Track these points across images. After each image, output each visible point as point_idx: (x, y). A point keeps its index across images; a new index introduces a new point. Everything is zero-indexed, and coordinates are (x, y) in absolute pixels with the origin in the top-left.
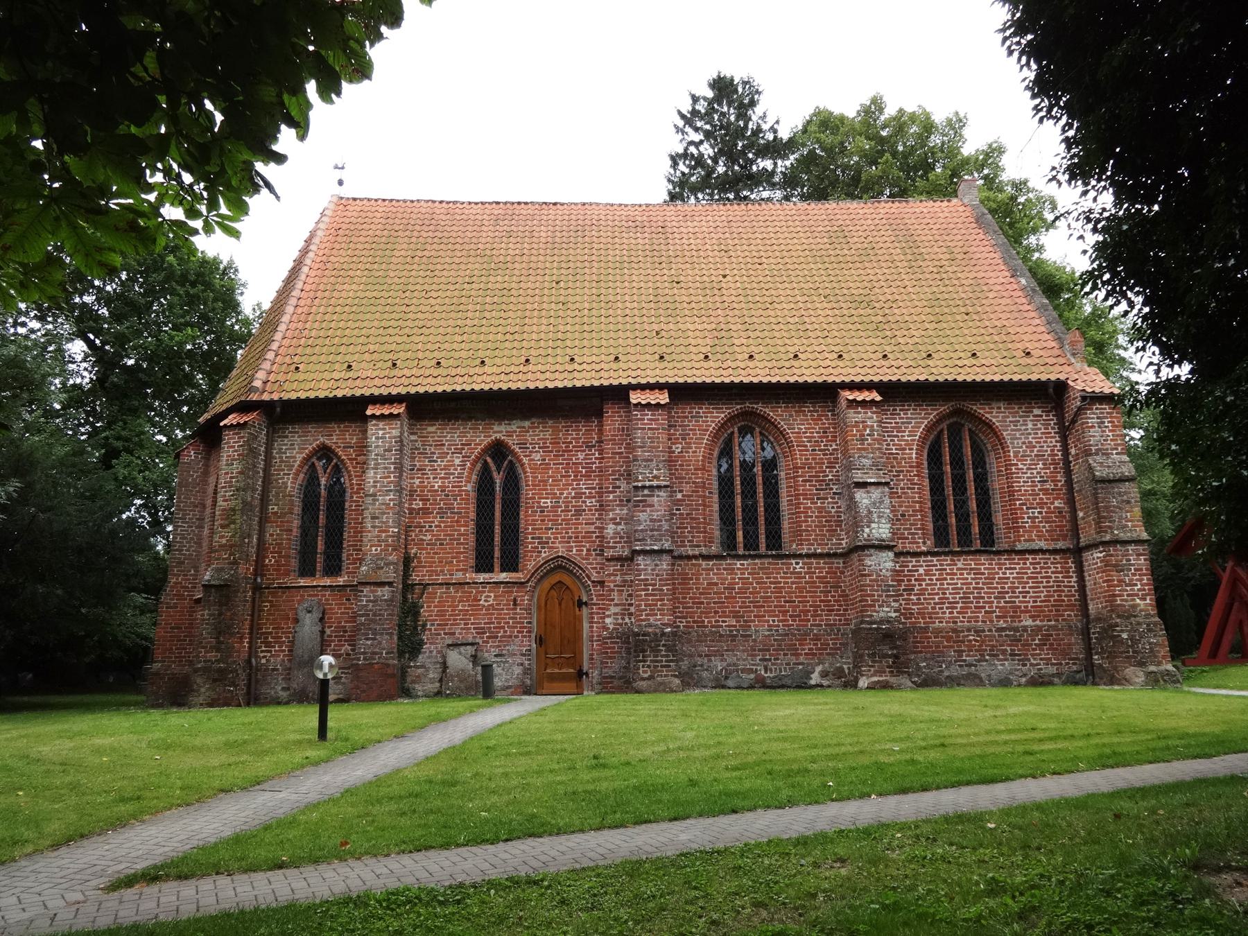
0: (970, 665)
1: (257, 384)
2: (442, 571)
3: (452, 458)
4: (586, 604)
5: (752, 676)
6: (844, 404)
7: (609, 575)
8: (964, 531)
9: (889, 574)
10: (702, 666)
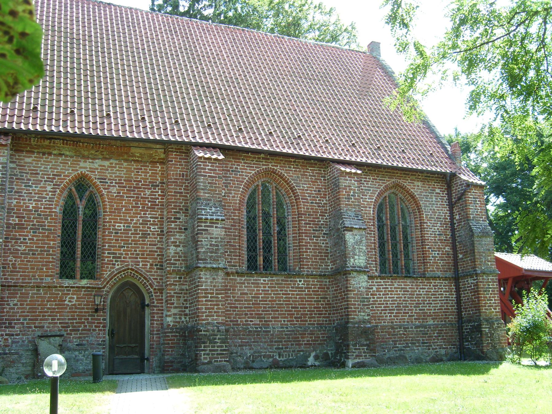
4: (148, 305)
5: (271, 360)
7: (171, 285)
10: (236, 353)
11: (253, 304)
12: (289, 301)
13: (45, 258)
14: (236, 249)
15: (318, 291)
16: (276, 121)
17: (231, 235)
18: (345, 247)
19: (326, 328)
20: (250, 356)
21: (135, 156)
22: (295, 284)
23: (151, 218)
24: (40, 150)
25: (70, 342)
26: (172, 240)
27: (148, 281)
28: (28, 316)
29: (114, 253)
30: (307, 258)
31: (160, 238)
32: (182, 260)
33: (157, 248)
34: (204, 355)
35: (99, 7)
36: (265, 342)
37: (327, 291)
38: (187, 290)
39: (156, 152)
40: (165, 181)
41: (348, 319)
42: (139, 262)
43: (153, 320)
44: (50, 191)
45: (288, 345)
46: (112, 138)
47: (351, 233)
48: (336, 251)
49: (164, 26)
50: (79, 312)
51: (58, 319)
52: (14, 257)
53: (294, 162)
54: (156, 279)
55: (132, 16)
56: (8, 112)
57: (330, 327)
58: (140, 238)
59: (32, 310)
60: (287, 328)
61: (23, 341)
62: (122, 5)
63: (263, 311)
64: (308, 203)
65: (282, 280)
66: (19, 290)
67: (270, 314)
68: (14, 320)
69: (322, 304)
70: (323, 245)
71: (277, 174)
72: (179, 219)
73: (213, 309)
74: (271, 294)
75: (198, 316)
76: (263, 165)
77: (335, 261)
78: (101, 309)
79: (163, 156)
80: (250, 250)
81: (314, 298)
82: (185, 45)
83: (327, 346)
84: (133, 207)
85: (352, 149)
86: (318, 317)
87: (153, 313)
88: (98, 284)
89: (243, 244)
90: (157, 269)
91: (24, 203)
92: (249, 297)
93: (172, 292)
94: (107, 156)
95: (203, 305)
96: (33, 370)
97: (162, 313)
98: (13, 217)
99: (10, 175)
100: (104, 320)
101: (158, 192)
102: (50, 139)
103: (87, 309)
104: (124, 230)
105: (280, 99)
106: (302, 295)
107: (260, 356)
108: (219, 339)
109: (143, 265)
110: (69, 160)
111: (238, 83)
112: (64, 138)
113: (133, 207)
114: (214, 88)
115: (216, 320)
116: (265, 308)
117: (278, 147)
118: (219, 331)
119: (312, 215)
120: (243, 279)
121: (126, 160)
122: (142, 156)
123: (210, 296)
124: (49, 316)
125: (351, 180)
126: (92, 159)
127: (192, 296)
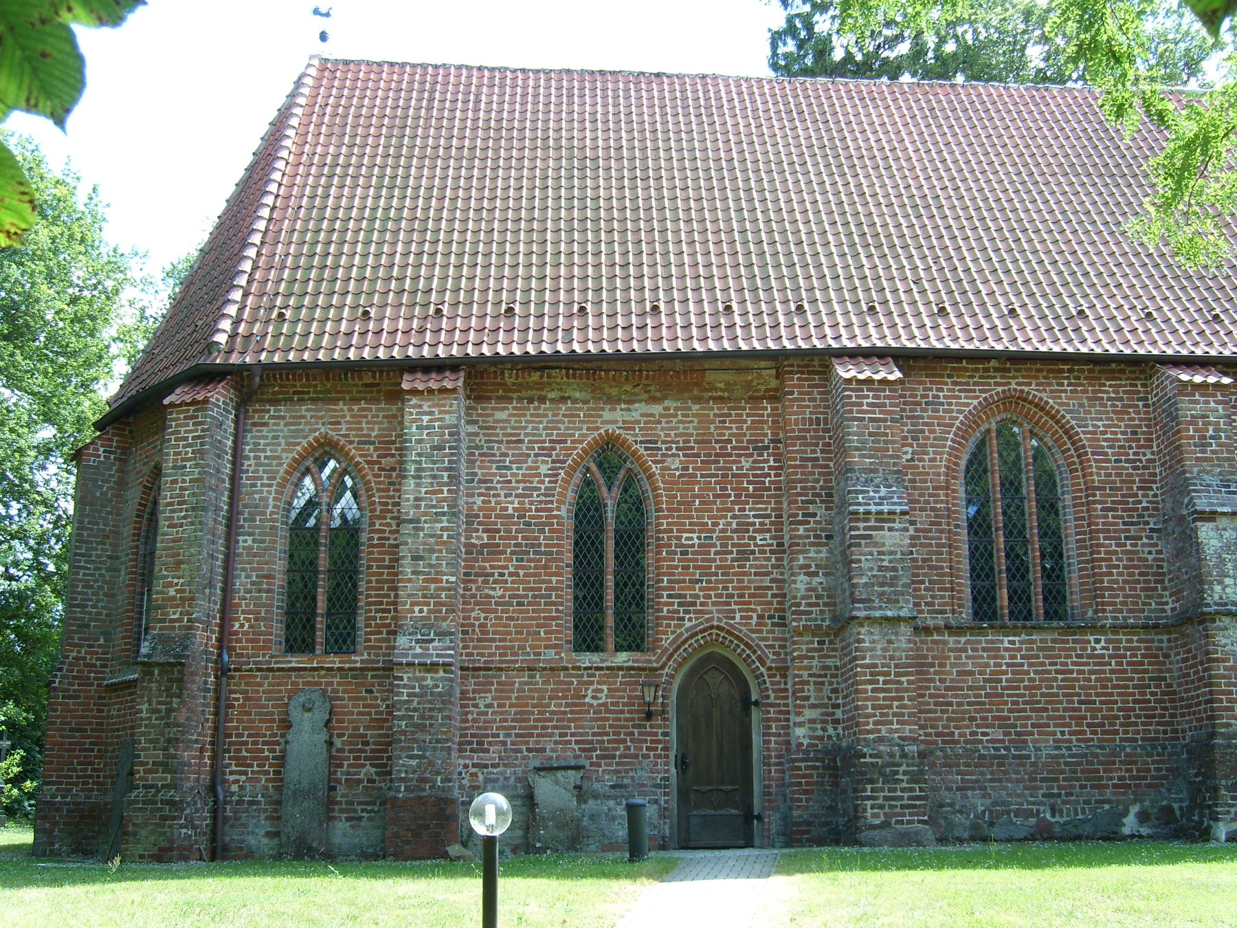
1: (221, 338)
2: (522, 648)
3: (533, 466)
4: (756, 703)
5: (1033, 821)
7: (801, 657)
8: (1019, 598)
10: (952, 805)
11: (987, 695)
12: (1073, 687)
13: (544, 611)
14: (943, 575)
15: (1142, 663)
16: (1025, 283)
17: (930, 545)
18: (1200, 560)
19: (1164, 748)
20: (983, 812)
21: (716, 389)
22: (1085, 649)
23: (754, 516)
24: (524, 394)
25: (598, 780)
26: (801, 562)
27: (754, 652)
28: (515, 728)
29: (680, 596)
30: (1112, 589)
31: (777, 559)
32: (825, 604)
33: (772, 581)
34: (872, 807)
35: (637, 84)
36: (1018, 781)
37: (1164, 663)
38: (837, 668)
39: (760, 376)
40: (781, 436)
41: (1214, 726)
42: (734, 611)
43: (769, 735)
44: (546, 476)
45: (1073, 787)
46: (663, 356)
47: (1211, 525)
48: (1179, 569)
49: (776, 104)
50: (614, 719)
51: (573, 735)
52: (483, 611)
53: (1069, 371)
54: (772, 647)
55: (706, 92)
56: (458, 325)
57: (1174, 746)
58: (733, 560)
59: (522, 717)
60: (1069, 749)
61: (506, 779)
62: (684, 72)
63: (1010, 711)
64: (1108, 461)
65: (1054, 641)
66: (494, 677)
67: (1029, 718)
68: (487, 736)
69: (1152, 694)
70: (1150, 557)
71: (1031, 403)
72: (814, 515)
73: (890, 707)
74: (1028, 673)
75: (858, 725)
76: (996, 384)
77: (1180, 591)
78: (657, 713)
79: (774, 383)
80: (978, 576)
81: (1132, 679)
82: (820, 138)
83: (1169, 790)
84: (715, 496)
85: (1211, 328)
86: (1143, 724)
87: (768, 720)
88: (649, 661)
89: (959, 562)
90: (774, 624)
91: (497, 503)
92: (977, 680)
93: (805, 674)
94: (658, 394)
95: (867, 699)
96: (525, 837)
97: (788, 720)
98: (477, 530)
99: (469, 448)
100: (666, 734)
101: (768, 461)
102: (541, 369)
103: (630, 712)
104: (700, 546)
105: (1037, 231)
106: (1104, 672)
107: (1008, 813)
108: (905, 773)
109: (742, 618)
110: (580, 409)
111: (940, 207)
112: (570, 365)
113: (715, 496)
114: (885, 225)
115: (897, 731)
116: (1016, 703)
117: (1028, 340)
118: (904, 755)
119: (1121, 489)
120: (963, 639)
121: (697, 400)
122: (729, 387)
123: (881, 679)
124: (555, 727)
125: (1207, 402)
126: (625, 402)
127: (845, 681)
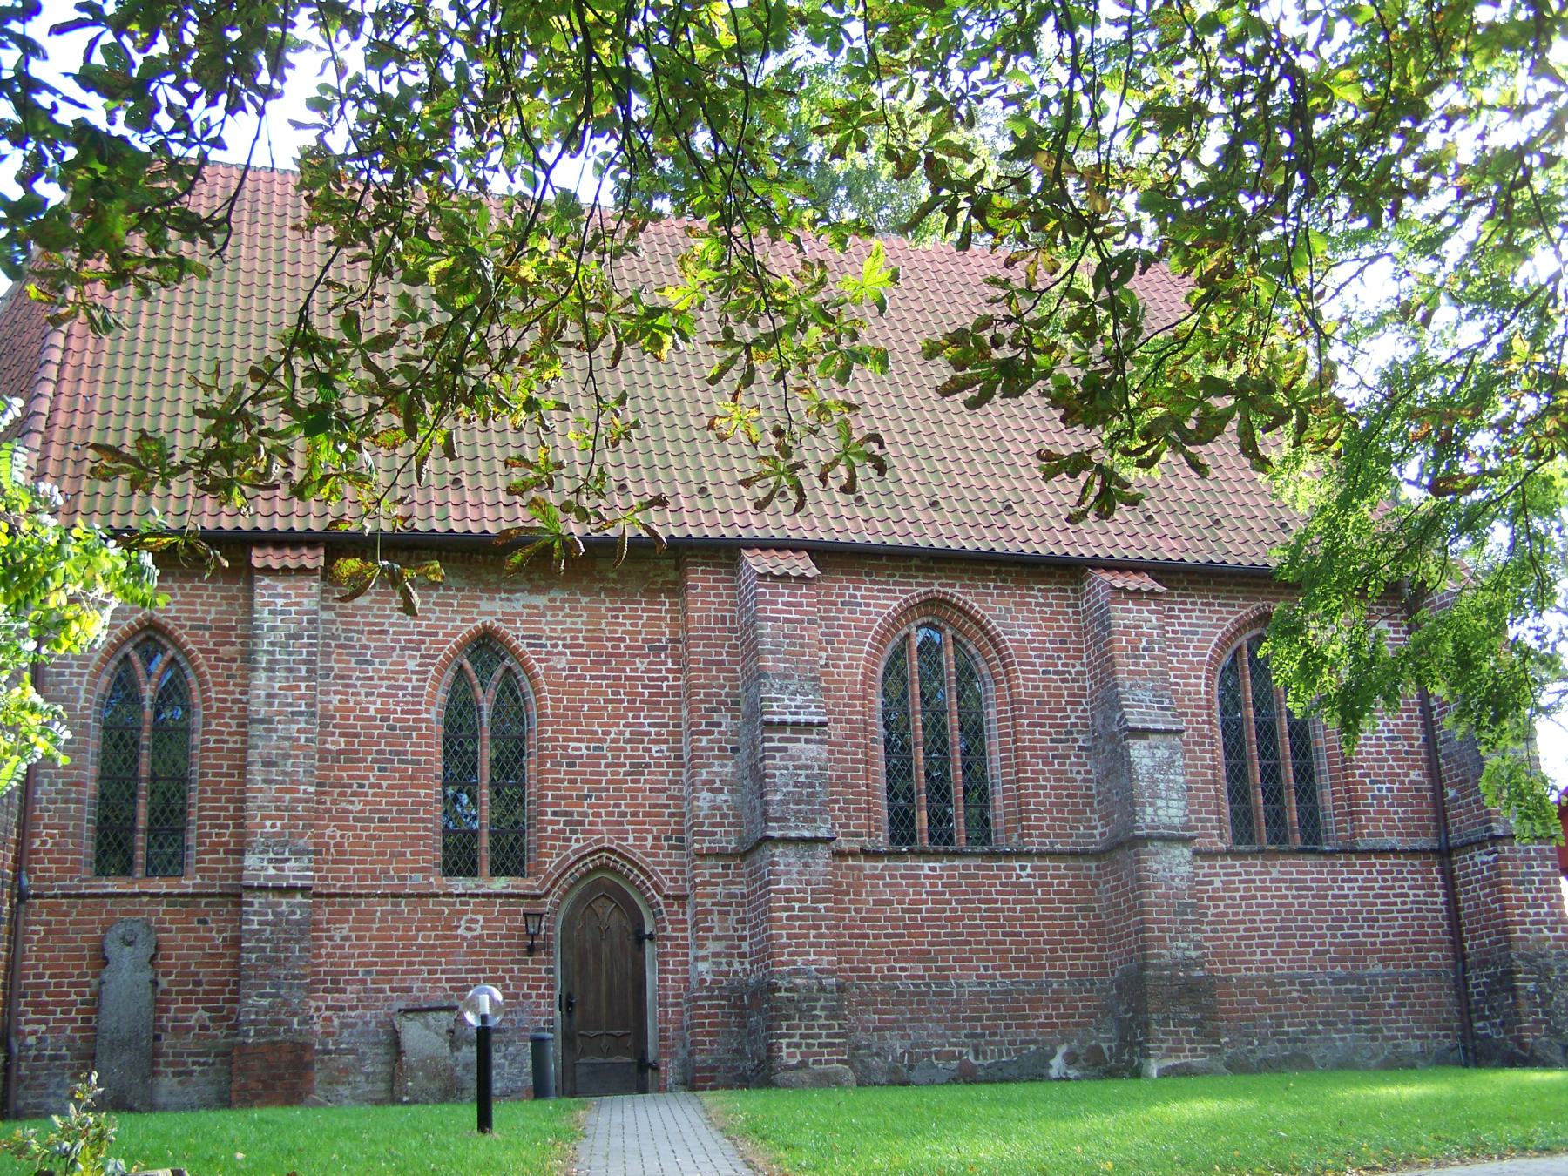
0: (1294, 1040)
2: (385, 871)
4: (651, 937)
5: (955, 1063)
6: (1103, 596)
8: (1276, 818)
9: (1184, 885)
10: (869, 1047)
